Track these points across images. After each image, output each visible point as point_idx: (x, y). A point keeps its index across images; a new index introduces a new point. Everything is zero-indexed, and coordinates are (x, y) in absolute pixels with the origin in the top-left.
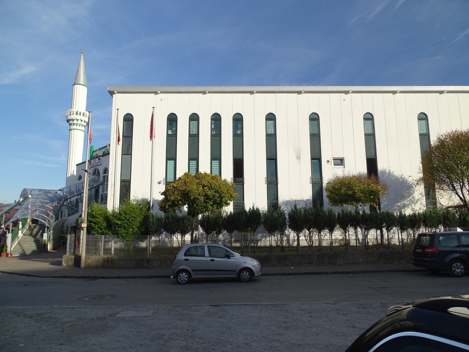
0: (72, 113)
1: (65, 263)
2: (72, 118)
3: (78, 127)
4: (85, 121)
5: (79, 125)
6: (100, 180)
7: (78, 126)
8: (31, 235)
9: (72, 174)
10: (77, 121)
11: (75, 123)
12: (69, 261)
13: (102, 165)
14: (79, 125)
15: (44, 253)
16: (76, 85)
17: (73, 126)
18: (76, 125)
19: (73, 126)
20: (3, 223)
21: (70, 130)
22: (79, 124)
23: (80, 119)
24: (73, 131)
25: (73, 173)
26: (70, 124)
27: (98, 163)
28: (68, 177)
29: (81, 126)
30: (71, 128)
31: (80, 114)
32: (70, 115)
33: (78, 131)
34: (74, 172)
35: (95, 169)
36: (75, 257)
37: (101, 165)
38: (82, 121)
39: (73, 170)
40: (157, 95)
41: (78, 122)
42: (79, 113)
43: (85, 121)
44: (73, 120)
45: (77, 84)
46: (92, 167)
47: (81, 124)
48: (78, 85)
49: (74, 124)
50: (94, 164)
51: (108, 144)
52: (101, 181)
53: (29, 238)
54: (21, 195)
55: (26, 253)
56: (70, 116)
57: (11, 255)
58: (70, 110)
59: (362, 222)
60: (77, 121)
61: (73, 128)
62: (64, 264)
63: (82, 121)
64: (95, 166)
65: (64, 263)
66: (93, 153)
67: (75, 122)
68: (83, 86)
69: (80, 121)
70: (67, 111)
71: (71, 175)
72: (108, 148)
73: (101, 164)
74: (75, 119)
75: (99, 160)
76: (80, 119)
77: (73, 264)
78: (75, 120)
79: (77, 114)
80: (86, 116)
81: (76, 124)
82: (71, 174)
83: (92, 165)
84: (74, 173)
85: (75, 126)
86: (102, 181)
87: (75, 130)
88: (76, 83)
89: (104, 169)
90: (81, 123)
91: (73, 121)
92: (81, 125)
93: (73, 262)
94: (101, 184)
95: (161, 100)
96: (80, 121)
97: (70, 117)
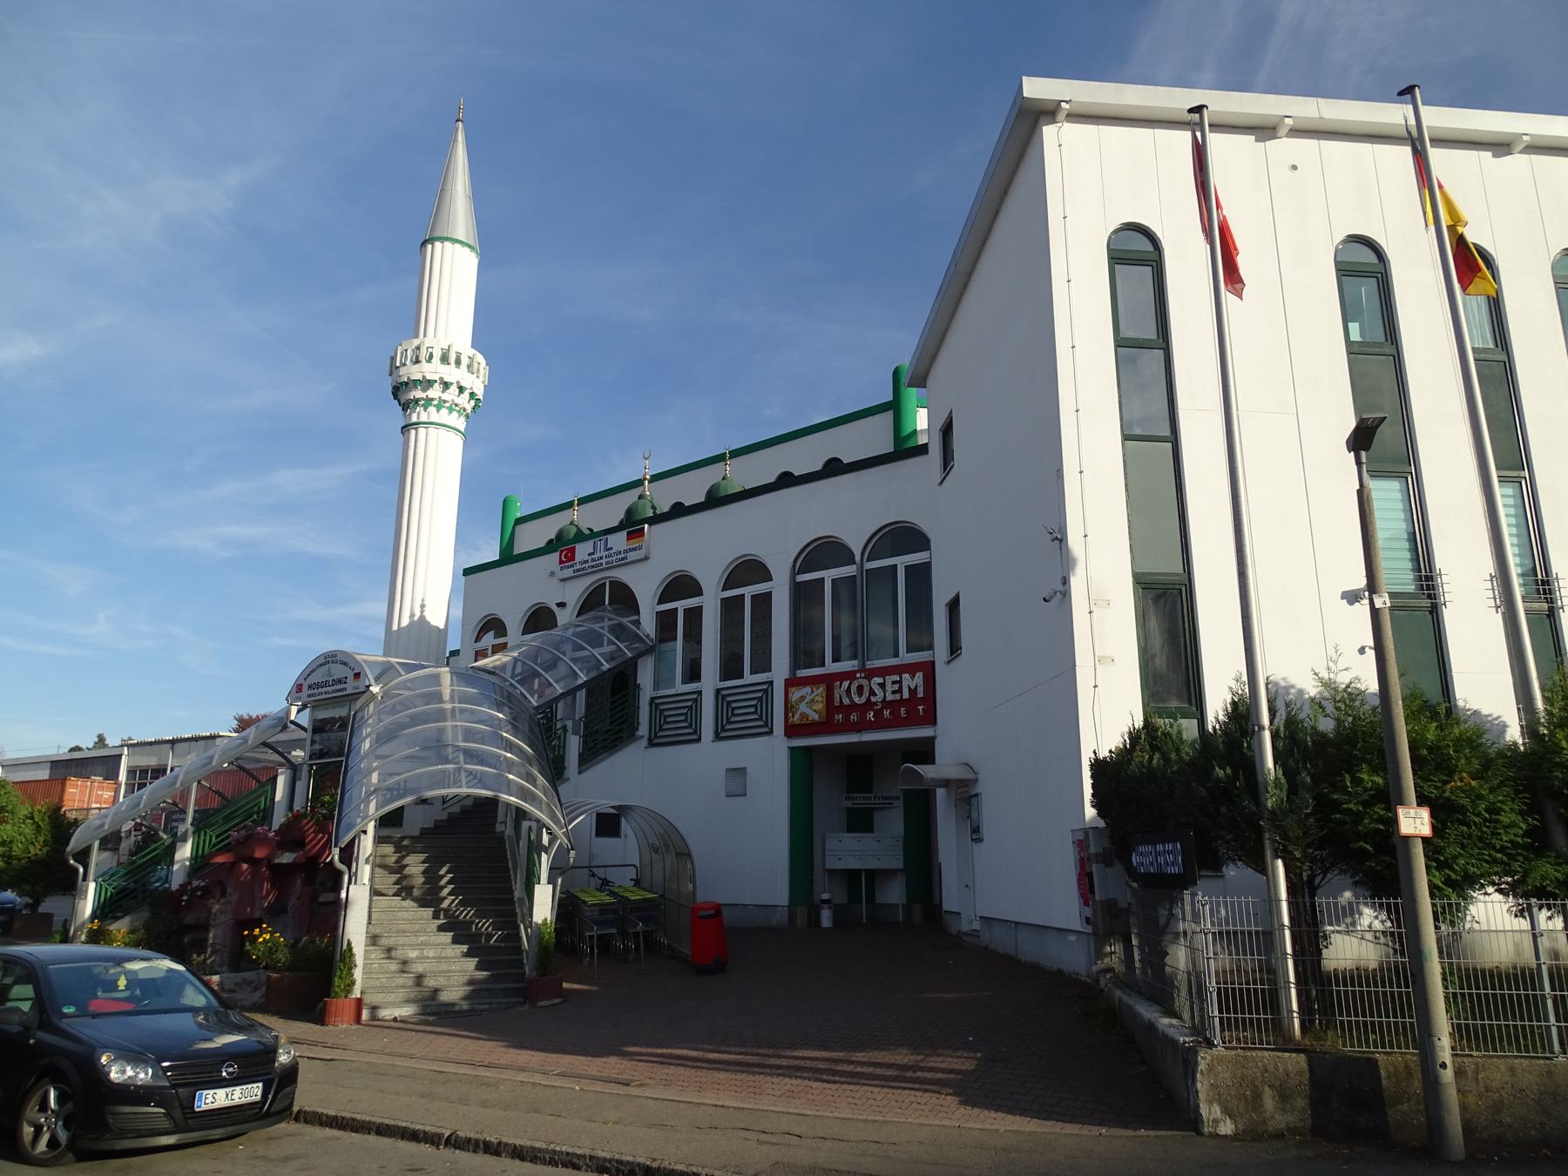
0: (423, 354)
1: (1227, 1111)
2: (424, 377)
3: (443, 416)
4: (472, 395)
5: (451, 410)
6: (639, 629)
7: (444, 411)
8: (404, 891)
9: (416, 618)
10: (443, 392)
11: (432, 400)
12: (1257, 1096)
13: (649, 561)
14: (451, 410)
15: (549, 999)
16: (438, 245)
17: (425, 410)
18: (439, 408)
19: (425, 410)
20: (191, 829)
21: (406, 428)
22: (447, 405)
23: (455, 385)
24: (422, 431)
25: (422, 611)
26: (406, 406)
27: (626, 551)
28: (395, 627)
29: (457, 414)
30: (414, 418)
31: (458, 362)
32: (417, 361)
33: (442, 431)
34: (425, 609)
35: (597, 581)
36: (1310, 1062)
37: (644, 563)
38: (461, 389)
39: (423, 600)
40: (1267, 143)
41: (445, 396)
42: (453, 358)
43: (472, 395)
44: (428, 384)
45: (443, 239)
46: (579, 576)
47: (456, 405)
48: (447, 244)
49: (429, 401)
50: (593, 560)
51: (648, 477)
52: (648, 636)
53: (402, 909)
54: (299, 688)
55: (445, 997)
56: (417, 365)
57: (374, 1008)
58: (416, 342)
59: (1299, 864)
60: (443, 392)
61: (424, 417)
62: (1216, 1122)
63: (461, 389)
64: (604, 566)
65: (1217, 1111)
66: (517, 528)
67: (435, 392)
68: (467, 250)
69: (454, 389)
70: (401, 345)
71: (412, 623)
72: (648, 493)
73: (646, 558)
74: (436, 381)
75: (628, 540)
76: (458, 382)
77: (1309, 1123)
78: (436, 385)
79: (445, 359)
80: (478, 370)
81: (435, 402)
82: (412, 615)
83: (578, 567)
84: (425, 613)
85: (432, 409)
86: (653, 635)
87: (432, 430)
88: (437, 234)
89: (481, 620)
90: (457, 401)
91: (425, 390)
92: (457, 409)
93: (1300, 1103)
94: (650, 650)
95: (1294, 167)
96: (454, 389)
97: (415, 372)
